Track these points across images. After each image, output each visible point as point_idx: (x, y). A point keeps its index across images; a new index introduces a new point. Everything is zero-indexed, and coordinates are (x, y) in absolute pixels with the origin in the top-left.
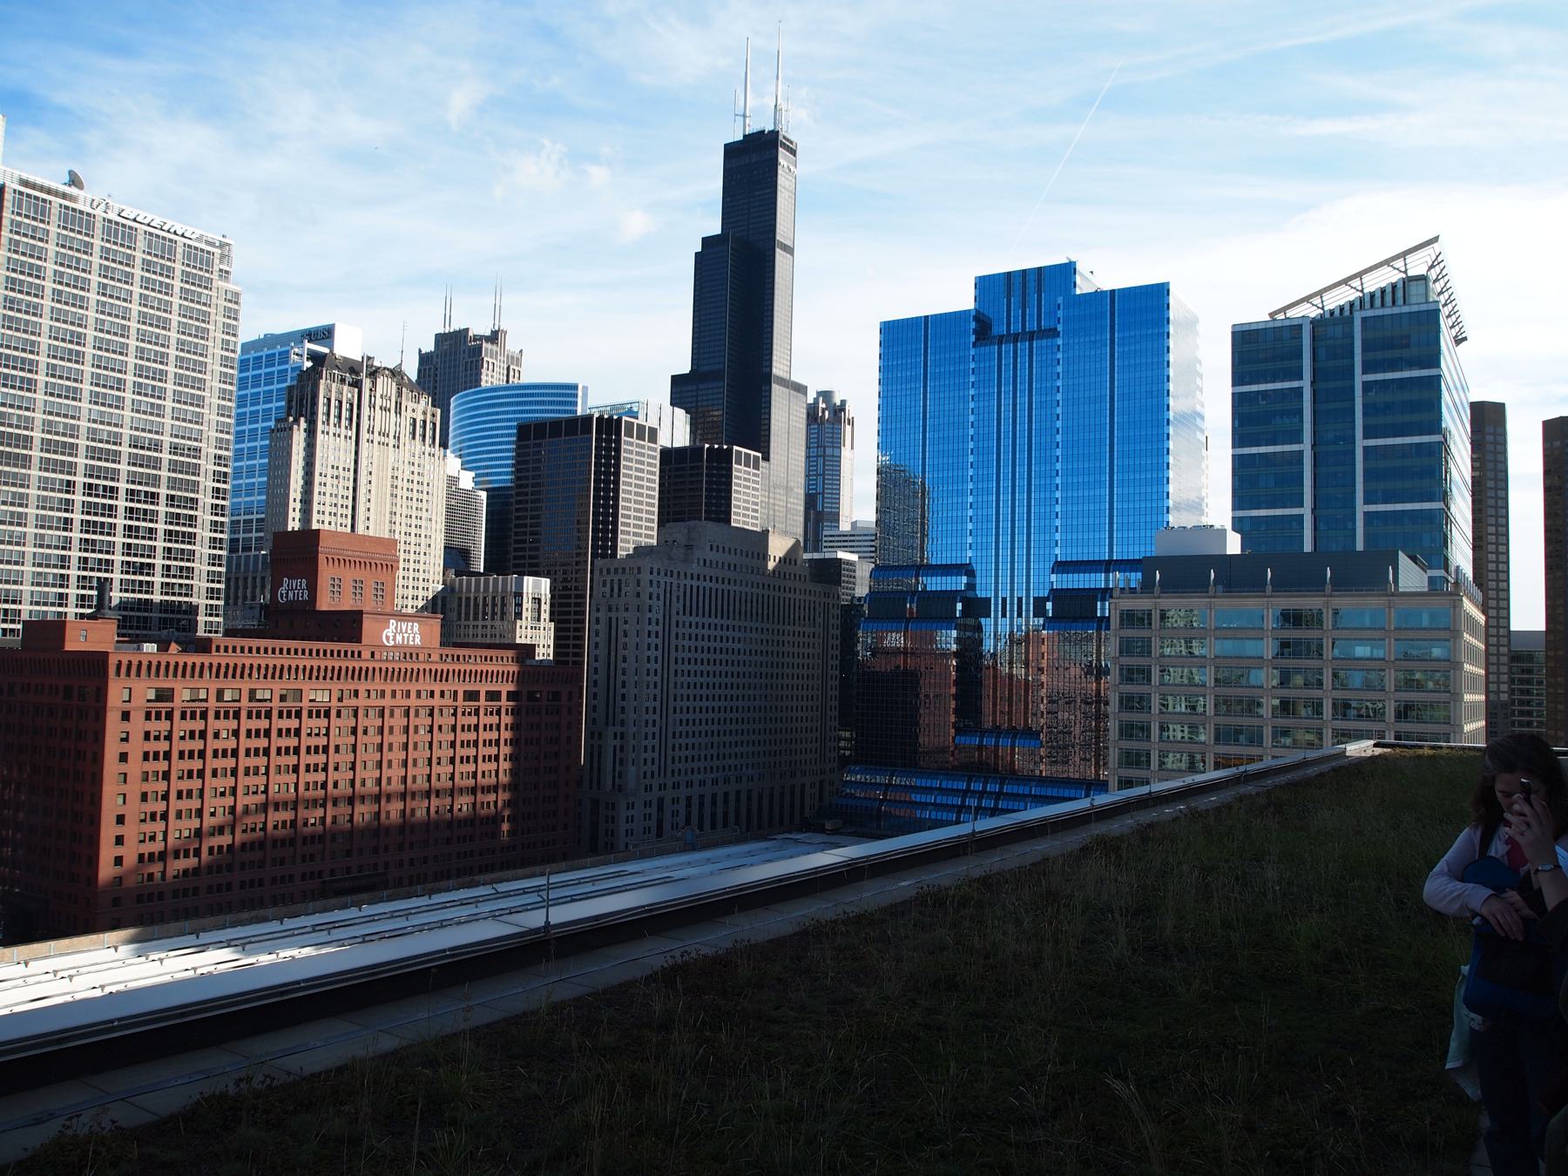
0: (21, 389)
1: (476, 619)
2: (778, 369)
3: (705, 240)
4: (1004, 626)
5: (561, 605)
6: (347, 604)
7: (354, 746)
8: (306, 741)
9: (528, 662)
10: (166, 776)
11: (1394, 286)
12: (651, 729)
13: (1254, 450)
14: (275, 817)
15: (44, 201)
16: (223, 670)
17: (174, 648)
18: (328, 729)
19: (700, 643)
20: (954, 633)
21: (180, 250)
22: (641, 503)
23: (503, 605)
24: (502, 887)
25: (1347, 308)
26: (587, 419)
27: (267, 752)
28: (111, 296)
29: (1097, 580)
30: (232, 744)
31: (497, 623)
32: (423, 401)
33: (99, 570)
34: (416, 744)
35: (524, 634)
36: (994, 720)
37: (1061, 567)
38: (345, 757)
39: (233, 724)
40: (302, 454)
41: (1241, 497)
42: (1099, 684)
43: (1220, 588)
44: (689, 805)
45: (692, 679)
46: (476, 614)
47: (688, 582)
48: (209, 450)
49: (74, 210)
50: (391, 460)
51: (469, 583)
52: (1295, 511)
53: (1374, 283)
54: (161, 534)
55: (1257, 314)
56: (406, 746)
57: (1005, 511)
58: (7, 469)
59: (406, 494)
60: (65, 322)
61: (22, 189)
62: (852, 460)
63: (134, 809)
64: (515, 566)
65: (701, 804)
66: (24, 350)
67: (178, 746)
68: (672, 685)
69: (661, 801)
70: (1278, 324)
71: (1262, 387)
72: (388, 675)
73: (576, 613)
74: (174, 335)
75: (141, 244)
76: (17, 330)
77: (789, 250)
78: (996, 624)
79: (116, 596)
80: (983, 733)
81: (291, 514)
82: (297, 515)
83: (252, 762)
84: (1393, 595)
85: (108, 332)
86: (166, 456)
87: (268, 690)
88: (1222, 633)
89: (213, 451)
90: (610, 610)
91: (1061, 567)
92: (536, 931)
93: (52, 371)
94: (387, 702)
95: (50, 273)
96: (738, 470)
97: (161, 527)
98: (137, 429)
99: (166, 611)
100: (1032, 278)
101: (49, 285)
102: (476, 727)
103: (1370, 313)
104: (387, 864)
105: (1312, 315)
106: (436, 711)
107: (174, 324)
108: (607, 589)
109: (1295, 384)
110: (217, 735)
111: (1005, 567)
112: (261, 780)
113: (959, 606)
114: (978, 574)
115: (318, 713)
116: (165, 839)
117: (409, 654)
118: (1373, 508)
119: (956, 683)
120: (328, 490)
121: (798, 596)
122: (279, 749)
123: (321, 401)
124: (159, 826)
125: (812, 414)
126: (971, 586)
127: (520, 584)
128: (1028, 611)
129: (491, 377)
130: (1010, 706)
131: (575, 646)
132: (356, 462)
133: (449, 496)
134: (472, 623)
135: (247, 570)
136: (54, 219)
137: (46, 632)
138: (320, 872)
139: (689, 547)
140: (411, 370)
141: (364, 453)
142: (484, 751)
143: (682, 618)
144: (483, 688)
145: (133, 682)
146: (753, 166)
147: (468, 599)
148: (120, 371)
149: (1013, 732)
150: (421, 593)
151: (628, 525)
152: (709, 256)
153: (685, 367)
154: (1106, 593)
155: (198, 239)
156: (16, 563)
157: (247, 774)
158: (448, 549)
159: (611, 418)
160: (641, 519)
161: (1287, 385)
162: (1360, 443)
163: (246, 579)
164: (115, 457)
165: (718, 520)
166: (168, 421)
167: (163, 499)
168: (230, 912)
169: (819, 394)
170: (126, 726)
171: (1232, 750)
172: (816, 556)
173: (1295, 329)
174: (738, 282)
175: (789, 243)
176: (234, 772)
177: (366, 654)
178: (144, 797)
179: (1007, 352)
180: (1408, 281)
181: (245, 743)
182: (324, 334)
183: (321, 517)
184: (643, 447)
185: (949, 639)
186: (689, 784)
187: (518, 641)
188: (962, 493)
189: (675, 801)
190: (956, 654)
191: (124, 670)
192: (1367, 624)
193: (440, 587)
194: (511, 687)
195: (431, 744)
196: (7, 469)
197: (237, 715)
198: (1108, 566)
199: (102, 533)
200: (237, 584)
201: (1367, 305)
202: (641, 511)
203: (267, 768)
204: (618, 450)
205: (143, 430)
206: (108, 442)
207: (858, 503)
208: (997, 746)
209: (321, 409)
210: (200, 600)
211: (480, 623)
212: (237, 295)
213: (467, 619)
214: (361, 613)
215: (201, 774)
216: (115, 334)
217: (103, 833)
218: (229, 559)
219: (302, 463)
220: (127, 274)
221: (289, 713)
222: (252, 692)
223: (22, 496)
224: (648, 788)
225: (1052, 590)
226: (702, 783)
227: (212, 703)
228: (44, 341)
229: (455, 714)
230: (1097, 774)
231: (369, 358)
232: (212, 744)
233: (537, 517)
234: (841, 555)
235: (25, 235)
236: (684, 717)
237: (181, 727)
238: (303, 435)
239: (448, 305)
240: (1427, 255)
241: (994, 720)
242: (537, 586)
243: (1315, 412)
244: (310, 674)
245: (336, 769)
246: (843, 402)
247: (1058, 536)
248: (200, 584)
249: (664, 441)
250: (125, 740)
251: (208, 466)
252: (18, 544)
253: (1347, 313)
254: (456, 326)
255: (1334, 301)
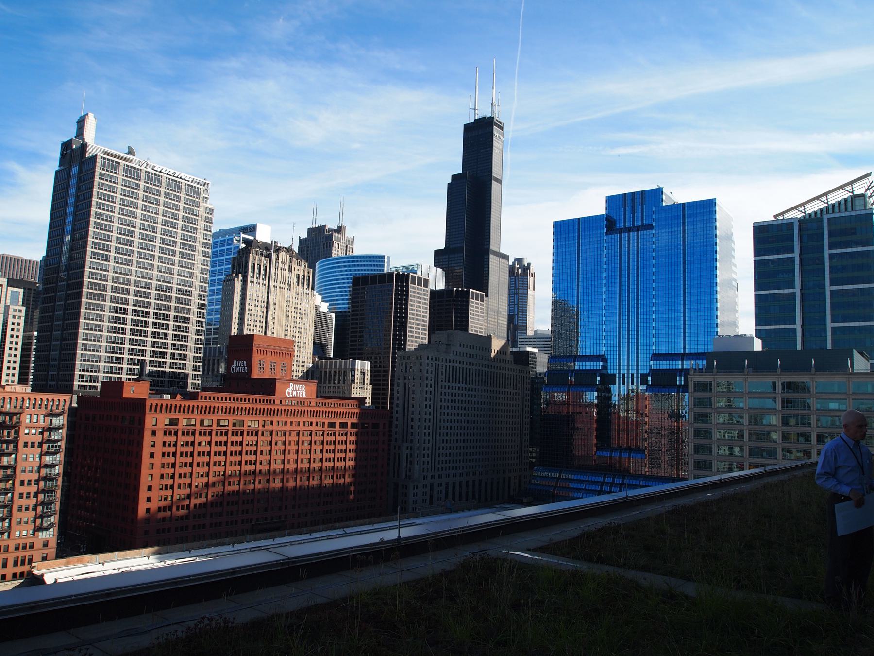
0: (102, 260)
1: (330, 383)
2: (493, 247)
4: (624, 390)
5: (375, 376)
7: (270, 451)
8: (246, 448)
10: (174, 465)
11: (846, 200)
12: (427, 445)
13: (767, 292)
17: (179, 397)
18: (257, 442)
19: (454, 398)
20: (596, 394)
21: (183, 187)
22: (419, 320)
23: (345, 375)
24: (348, 530)
25: (819, 212)
26: (391, 274)
27: (225, 453)
29: (677, 364)
30: (207, 449)
31: (342, 385)
32: (303, 265)
34: (302, 451)
35: (356, 391)
37: (656, 357)
39: (208, 438)
40: (240, 293)
41: (760, 318)
42: (678, 423)
43: (751, 369)
44: (447, 488)
45: (449, 418)
46: (330, 380)
48: (196, 292)
50: (286, 296)
51: (326, 363)
52: (791, 326)
53: (834, 199)
54: (170, 336)
55: (767, 216)
57: (624, 325)
59: (293, 315)
62: (534, 296)
63: (157, 483)
64: (351, 354)
65: (454, 487)
66: (104, 240)
69: (432, 485)
70: (780, 222)
71: (771, 257)
72: (289, 413)
73: (384, 380)
74: (179, 231)
75: (164, 184)
76: (101, 229)
77: (499, 181)
78: (619, 389)
79: (148, 369)
80: (612, 450)
81: (233, 326)
83: (217, 459)
84: (851, 374)
86: (174, 295)
87: (226, 421)
88: (751, 395)
89: (198, 292)
90: (405, 379)
91: (656, 357)
94: (288, 428)
95: (118, 200)
96: (473, 304)
97: (171, 332)
101: (118, 206)
102: (334, 442)
103: (833, 216)
104: (286, 516)
105: (799, 216)
108: (404, 368)
109: (790, 255)
110: (200, 444)
111: (624, 357)
113: (598, 378)
114: (609, 360)
115: (252, 433)
116: (207, 497)
117: (300, 401)
118: (836, 325)
119: (597, 421)
120: (253, 312)
121: (507, 372)
123: (250, 265)
125: (512, 269)
126: (605, 367)
127: (354, 364)
131: (383, 399)
132: (268, 298)
134: (327, 385)
135: (214, 356)
136: (121, 171)
137: (113, 387)
138: (251, 520)
139: (448, 345)
140: (296, 248)
142: (338, 455)
143: (444, 384)
144: (338, 421)
145: (159, 415)
146: (479, 137)
147: (326, 372)
149: (629, 450)
150: (300, 369)
152: (456, 186)
153: (442, 245)
154: (685, 372)
155: (192, 181)
156: (97, 351)
157: (215, 465)
158: (315, 343)
159: (403, 274)
161: (785, 256)
162: (828, 288)
165: (461, 330)
166: (175, 277)
167: (172, 318)
168: (204, 540)
169: (516, 260)
170: (154, 438)
171: (759, 461)
172: (514, 349)
173: (789, 224)
174: (471, 200)
175: (499, 178)
176: (208, 464)
177: (277, 402)
178: (162, 476)
179: (625, 237)
180: (854, 197)
181: (214, 448)
182: (252, 229)
183: (249, 327)
184: (421, 290)
185: (592, 397)
188: (600, 315)
189: (440, 485)
190: (597, 406)
191: (153, 408)
192: (836, 391)
194: (355, 421)
197: (210, 434)
198: (683, 356)
200: (208, 362)
201: (831, 211)
202: (419, 324)
203: (225, 462)
204: (407, 291)
207: (540, 319)
209: (250, 269)
210: (189, 371)
211: (332, 385)
212: (212, 210)
213: (325, 383)
214: (275, 379)
215: (191, 465)
218: (205, 349)
222: (219, 421)
224: (425, 478)
226: (455, 475)
227: (198, 427)
228: (114, 235)
229: (323, 435)
230: (678, 475)
233: (362, 328)
234: (529, 349)
236: (445, 438)
237: (182, 439)
239: (315, 213)
240: (865, 183)
242: (363, 365)
243: (802, 271)
244: (249, 412)
245: (261, 463)
246: (529, 264)
247: (654, 340)
249: (431, 286)
250: (153, 446)
251: (195, 300)
252: (98, 341)
253: (819, 216)
254: (319, 224)
255: (811, 208)
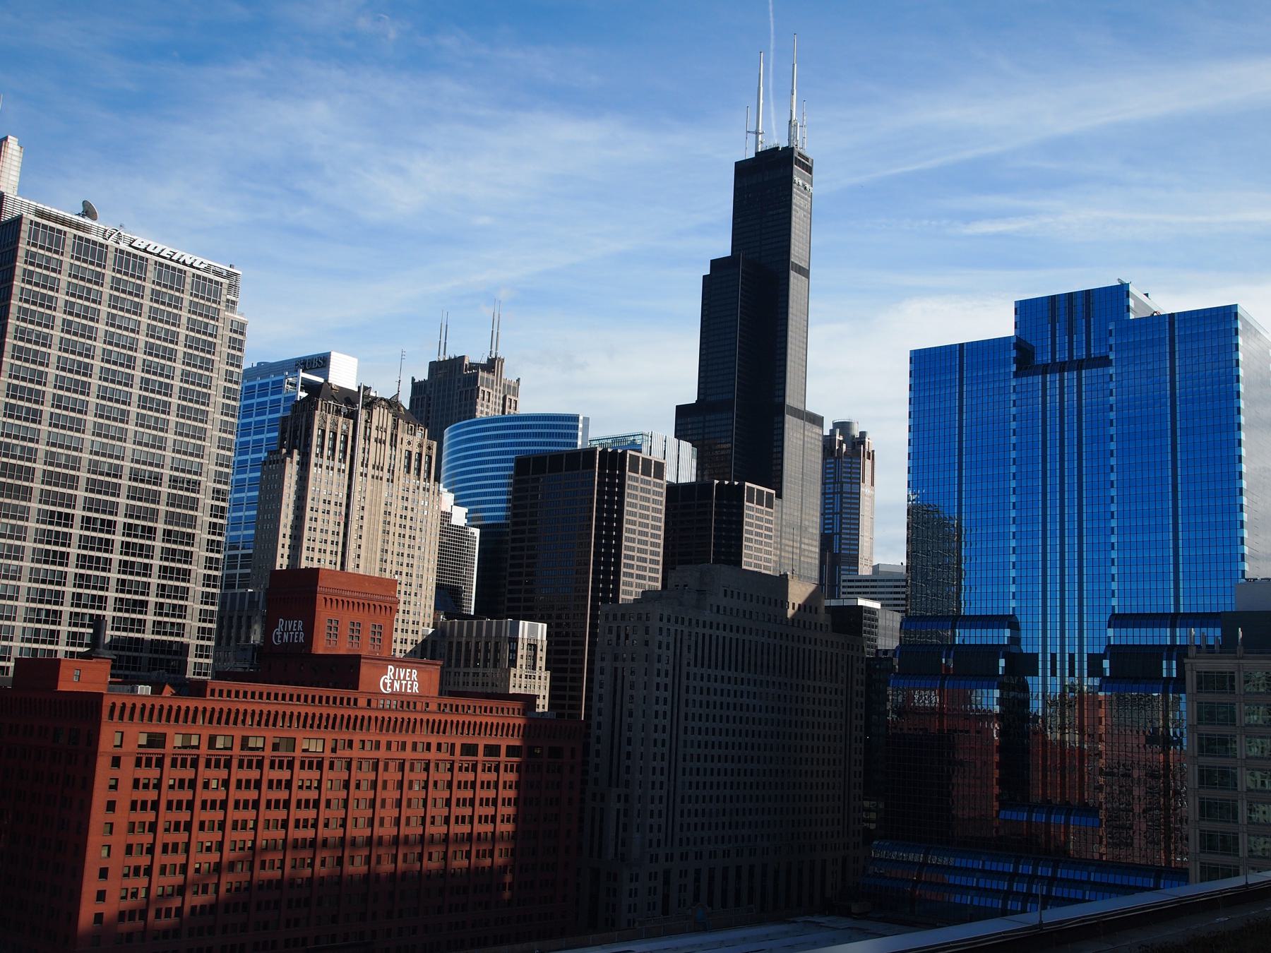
0: (26, 420)
1: (467, 665)
2: (790, 401)
3: (714, 263)
5: (557, 652)
6: (343, 648)
7: (346, 801)
8: (297, 794)
9: (530, 714)
10: (153, 827)
14: (227, 879)
15: (59, 231)
16: (216, 715)
17: (168, 690)
18: (320, 782)
20: (997, 693)
27: (256, 804)
28: (119, 327)
29: (1163, 636)
30: (221, 795)
31: (490, 670)
32: (419, 434)
33: (92, 607)
35: (518, 683)
36: (1044, 793)
37: (1118, 620)
38: (336, 813)
39: (223, 773)
42: (1167, 756)
44: (697, 880)
47: (700, 630)
48: (208, 483)
49: (88, 240)
51: (461, 626)
56: (399, 803)
58: (8, 501)
60: (73, 353)
61: (39, 220)
62: (872, 497)
63: (118, 863)
64: (509, 609)
66: (31, 381)
67: (167, 794)
68: (681, 743)
69: (667, 873)
72: (385, 725)
74: (179, 366)
75: (151, 274)
77: (805, 272)
81: (280, 551)
82: (286, 551)
83: (240, 815)
85: (115, 363)
89: (212, 485)
90: (616, 658)
91: (1118, 620)
92: (1035, 927)
93: (58, 402)
94: (382, 754)
95: (61, 304)
98: (138, 462)
99: (156, 651)
100: (1079, 303)
101: (59, 315)
102: (473, 784)
106: (432, 765)
107: (180, 355)
110: (206, 785)
112: (248, 835)
113: (1002, 662)
114: (1023, 626)
115: (311, 763)
116: (217, 891)
117: (406, 702)
119: (1000, 749)
120: (319, 525)
122: (269, 802)
124: (142, 881)
126: (1015, 640)
128: (1081, 669)
129: (486, 409)
130: (1063, 777)
133: (443, 533)
137: (38, 669)
141: (357, 487)
143: (693, 670)
144: (482, 742)
146: (766, 186)
147: (459, 644)
148: (124, 403)
150: (410, 637)
151: (631, 566)
152: (718, 281)
153: (691, 396)
158: (439, 587)
159: (615, 452)
160: (645, 560)
163: (231, 618)
164: (115, 490)
165: (728, 562)
169: (836, 425)
170: (116, 773)
172: (834, 603)
174: (749, 310)
175: (803, 265)
176: (222, 825)
177: (362, 702)
178: (129, 849)
181: (235, 794)
183: (311, 554)
184: (648, 483)
185: (991, 699)
186: (699, 855)
187: (512, 691)
188: (1004, 536)
190: (999, 717)
191: (117, 713)
193: (430, 631)
195: (425, 801)
196: (8, 501)
197: (228, 764)
198: (1174, 620)
199: (97, 569)
200: (228, 620)
202: (645, 551)
203: (256, 822)
205: (144, 463)
206: (108, 475)
207: (884, 543)
208: (1048, 824)
209: (315, 440)
210: (192, 641)
211: (472, 670)
212: (243, 325)
213: (458, 665)
214: (359, 657)
215: (188, 826)
216: (122, 365)
217: (85, 888)
218: (223, 596)
219: (293, 497)
220: (137, 305)
221: (281, 762)
222: (245, 740)
223: (20, 528)
225: (1109, 646)
227: (204, 750)
228: (52, 371)
229: (451, 770)
230: (1168, 861)
231: (366, 388)
232: (202, 795)
235: (39, 266)
238: (295, 467)
241: (1044, 793)
242: (533, 631)
244: (306, 722)
246: (863, 434)
248: (192, 623)
249: (670, 476)
250: (114, 787)
251: (206, 500)
252: (13, 578)
254: (452, 353)
